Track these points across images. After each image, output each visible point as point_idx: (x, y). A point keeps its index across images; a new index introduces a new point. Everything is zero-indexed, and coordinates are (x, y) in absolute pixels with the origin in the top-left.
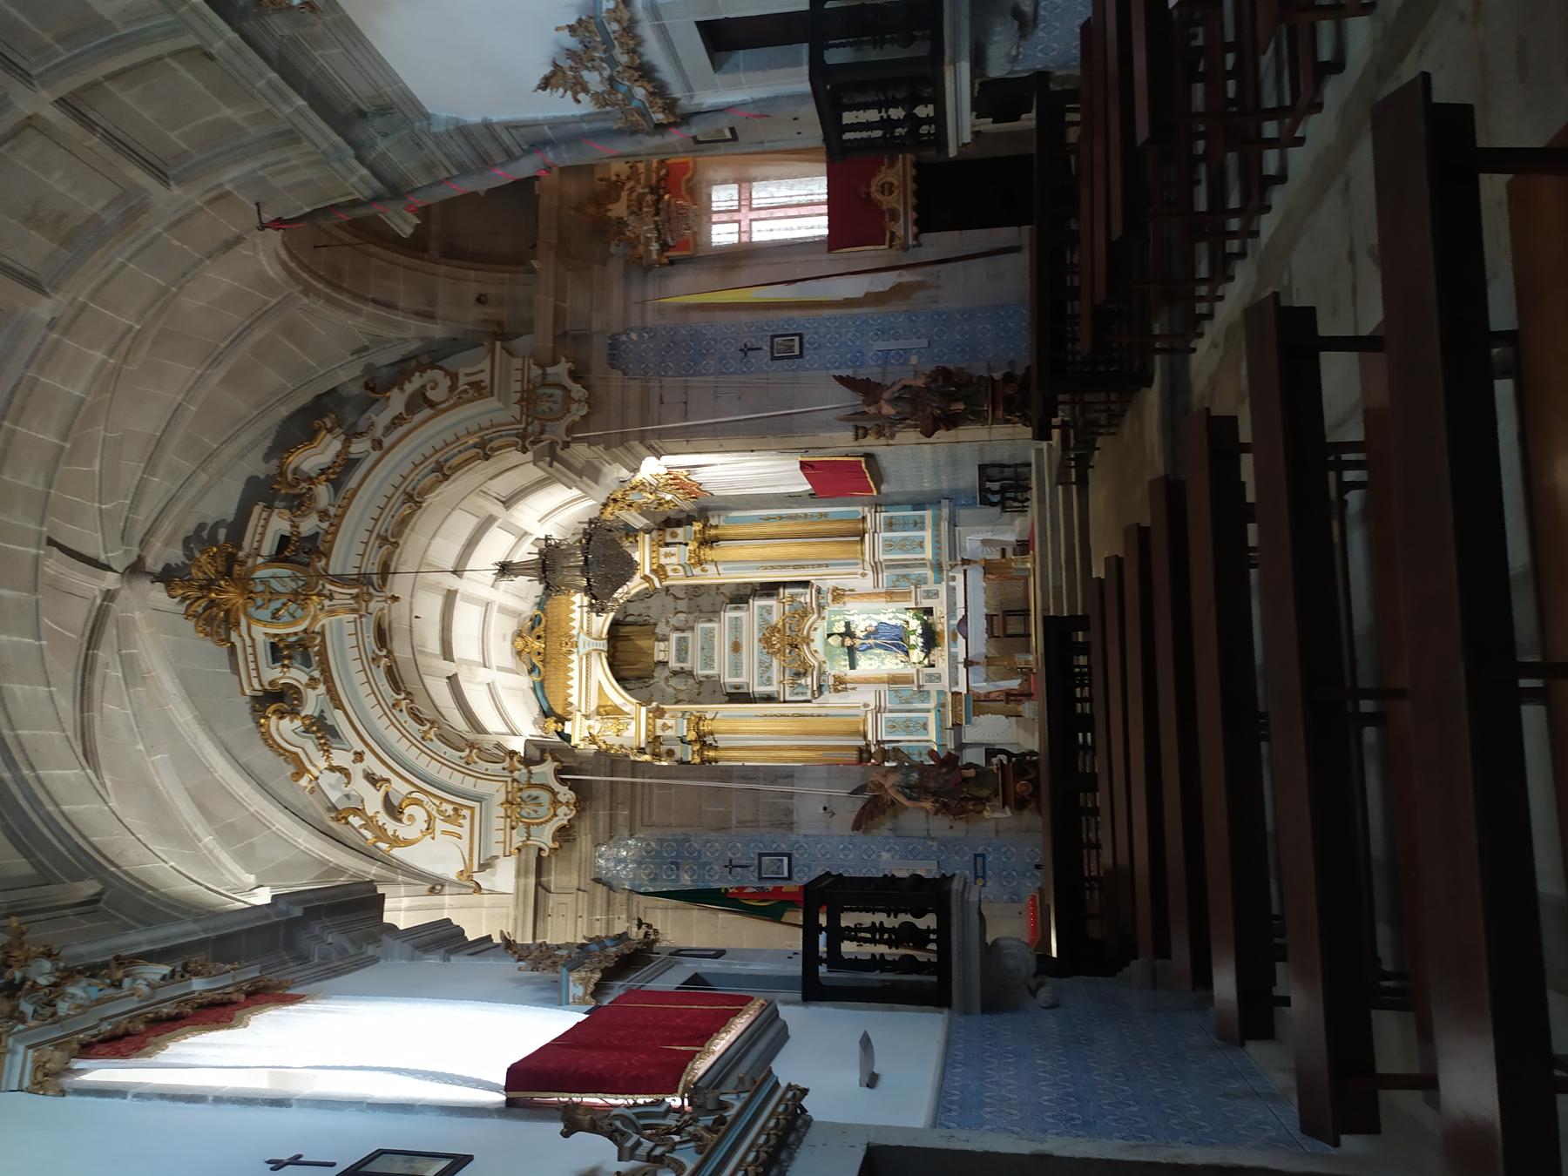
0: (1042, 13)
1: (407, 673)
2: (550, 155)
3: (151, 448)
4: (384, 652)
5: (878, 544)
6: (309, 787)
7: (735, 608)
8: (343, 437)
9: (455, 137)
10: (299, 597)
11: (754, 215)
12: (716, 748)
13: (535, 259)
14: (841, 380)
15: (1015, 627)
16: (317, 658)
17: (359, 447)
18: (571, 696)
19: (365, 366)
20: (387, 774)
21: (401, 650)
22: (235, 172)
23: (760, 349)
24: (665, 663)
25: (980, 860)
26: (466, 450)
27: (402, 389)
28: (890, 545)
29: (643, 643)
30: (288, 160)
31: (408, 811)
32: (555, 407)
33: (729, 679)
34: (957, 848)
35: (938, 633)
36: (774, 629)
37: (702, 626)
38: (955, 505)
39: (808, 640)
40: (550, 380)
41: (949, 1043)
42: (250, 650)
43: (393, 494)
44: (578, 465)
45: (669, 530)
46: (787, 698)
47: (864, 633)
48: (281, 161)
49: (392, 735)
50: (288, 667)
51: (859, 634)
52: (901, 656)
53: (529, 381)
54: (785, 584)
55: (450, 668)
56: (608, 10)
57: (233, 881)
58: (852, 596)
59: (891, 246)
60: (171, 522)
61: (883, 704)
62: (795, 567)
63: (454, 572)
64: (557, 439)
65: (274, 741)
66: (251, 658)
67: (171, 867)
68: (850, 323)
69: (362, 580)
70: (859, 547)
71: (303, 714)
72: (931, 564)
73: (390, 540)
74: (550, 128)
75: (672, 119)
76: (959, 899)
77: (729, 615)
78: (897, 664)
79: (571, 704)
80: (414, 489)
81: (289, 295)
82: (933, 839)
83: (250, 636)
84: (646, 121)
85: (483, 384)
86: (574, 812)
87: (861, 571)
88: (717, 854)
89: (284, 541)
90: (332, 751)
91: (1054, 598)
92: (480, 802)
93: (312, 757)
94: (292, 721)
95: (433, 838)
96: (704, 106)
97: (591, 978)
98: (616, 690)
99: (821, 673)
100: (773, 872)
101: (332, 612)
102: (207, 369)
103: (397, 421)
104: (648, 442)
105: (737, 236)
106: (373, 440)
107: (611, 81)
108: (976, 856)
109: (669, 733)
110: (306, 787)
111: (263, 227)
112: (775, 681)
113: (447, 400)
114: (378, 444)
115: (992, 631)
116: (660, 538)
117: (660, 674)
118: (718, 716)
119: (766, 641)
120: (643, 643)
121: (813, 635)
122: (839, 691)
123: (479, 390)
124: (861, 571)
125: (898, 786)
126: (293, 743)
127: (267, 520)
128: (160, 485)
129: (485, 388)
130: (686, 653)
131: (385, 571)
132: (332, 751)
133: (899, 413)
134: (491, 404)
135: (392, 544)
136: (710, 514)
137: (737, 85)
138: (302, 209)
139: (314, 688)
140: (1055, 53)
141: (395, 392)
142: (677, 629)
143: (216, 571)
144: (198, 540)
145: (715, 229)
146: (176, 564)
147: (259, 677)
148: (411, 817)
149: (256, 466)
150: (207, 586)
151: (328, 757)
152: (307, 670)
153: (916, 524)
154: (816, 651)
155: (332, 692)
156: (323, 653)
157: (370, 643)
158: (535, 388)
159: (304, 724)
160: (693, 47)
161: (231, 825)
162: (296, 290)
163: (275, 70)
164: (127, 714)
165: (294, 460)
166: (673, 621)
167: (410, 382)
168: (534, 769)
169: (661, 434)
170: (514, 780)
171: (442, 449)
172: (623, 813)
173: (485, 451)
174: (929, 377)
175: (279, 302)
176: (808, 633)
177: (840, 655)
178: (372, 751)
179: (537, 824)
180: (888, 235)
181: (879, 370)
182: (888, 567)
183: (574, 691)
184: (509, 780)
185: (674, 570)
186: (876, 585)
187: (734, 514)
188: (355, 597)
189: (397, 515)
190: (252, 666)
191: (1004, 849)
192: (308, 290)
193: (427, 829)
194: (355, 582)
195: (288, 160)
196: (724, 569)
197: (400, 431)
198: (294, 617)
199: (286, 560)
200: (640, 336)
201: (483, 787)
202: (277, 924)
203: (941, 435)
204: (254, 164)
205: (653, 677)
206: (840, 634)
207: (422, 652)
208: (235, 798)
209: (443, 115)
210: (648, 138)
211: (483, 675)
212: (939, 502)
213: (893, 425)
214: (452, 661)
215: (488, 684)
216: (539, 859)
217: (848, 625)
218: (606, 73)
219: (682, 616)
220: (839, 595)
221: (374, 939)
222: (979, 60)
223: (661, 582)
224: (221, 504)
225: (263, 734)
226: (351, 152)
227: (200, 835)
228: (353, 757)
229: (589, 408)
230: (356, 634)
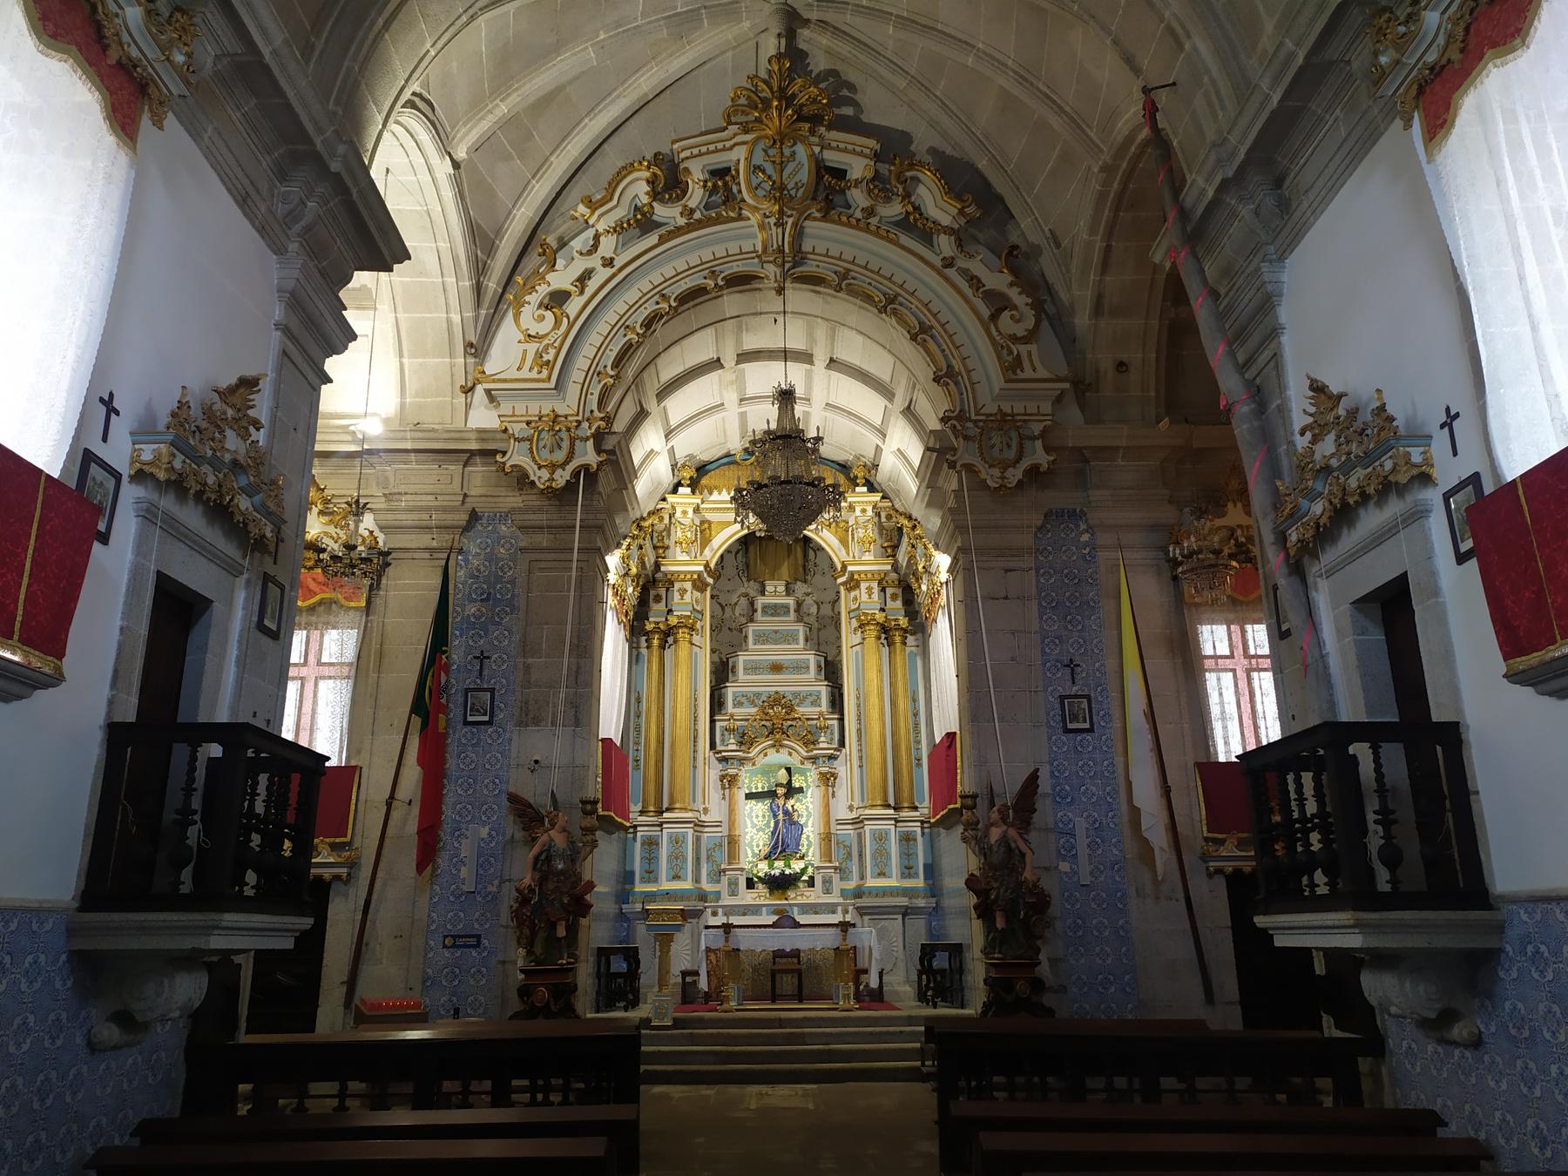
0: (1457, 1052)
1: (706, 311)
2: (1244, 409)
3: (924, 21)
4: (721, 283)
5: (882, 823)
6: (577, 215)
7: (819, 666)
8: (956, 226)
9: (1259, 294)
10: (779, 193)
11: (1241, 674)
12: (662, 647)
13: (1171, 422)
14: (1033, 778)
15: (787, 983)
16: (714, 215)
17: (945, 244)
18: (720, 494)
19: (1039, 246)
20: (589, 291)
21: (731, 302)
22: (1203, 48)
23: (1073, 682)
24: (763, 592)
25: (473, 941)
26: (946, 357)
27: (1011, 285)
28: (881, 837)
29: (785, 570)
30: (1223, 108)
31: (549, 314)
32: (996, 452)
33: (742, 660)
34: (489, 915)
36: (790, 708)
37: (801, 630)
38: (930, 914)
39: (778, 746)
40: (1027, 444)
41: (39, 912)
42: (720, 146)
43: (894, 283)
44: (940, 482)
45: (899, 591)
46: (718, 724)
48: (1220, 100)
49: (632, 295)
50: (705, 186)
51: (792, 802)
52: (767, 849)
53: (1025, 421)
54: (841, 720)
55: (729, 359)
56: (1409, 454)
57: (459, 135)
58: (826, 796)
59: (1206, 839)
60: (850, 52)
61: (707, 829)
62: (859, 730)
63: (832, 360)
64: (958, 454)
65: (625, 177)
66: (712, 147)
67: (428, 51)
68: (1108, 789)
69: (799, 257)
70: (879, 802)
71: (654, 204)
73: (844, 282)
74: (1278, 406)
75: (1292, 553)
76: (210, 923)
77: (812, 659)
78: (758, 846)
79: (711, 493)
80: (901, 304)
81: (1101, 151)
82: (500, 886)
83: (735, 145)
84: (1286, 519)
85: (1018, 371)
86: (542, 487)
88: (496, 643)
89: (840, 174)
90: (615, 236)
91: (790, 1033)
92: (555, 389)
93: (606, 216)
94: (647, 193)
95: (519, 342)
96: (1314, 594)
97: (160, 468)
98: (724, 543)
99: (742, 761)
100: (473, 704)
101: (762, 227)
102: (1013, 71)
103: (975, 282)
104: (961, 556)
105: (1212, 653)
106: (953, 258)
107: (1326, 470)
108: (478, 937)
109: (677, 596)
110: (576, 211)
111: (1146, 91)
112: (735, 710)
113: (1000, 334)
114: (949, 263)
115: (781, 957)
116: (890, 582)
117: (751, 588)
118: (696, 649)
119: (777, 700)
120: (785, 570)
121: (784, 751)
122: (722, 781)
123: (1013, 367)
125: (550, 847)
126: (622, 199)
127: (861, 154)
128: (887, 35)
129: (1015, 373)
130: (772, 615)
131: (814, 280)
132: (615, 236)
133: (991, 848)
134: (998, 381)
135: (840, 284)
136: (919, 635)
137: (1340, 633)
138: (1176, 137)
139: (681, 214)
140: (1409, 1067)
141: (1007, 277)
142: (799, 604)
143: (802, 106)
144: (838, 87)
145: (1221, 630)
146: (809, 64)
147: (693, 156)
148: (542, 318)
149: (923, 140)
150: (787, 99)
151: (608, 232)
152: (701, 207)
153: (909, 868)
154: (766, 755)
155: (679, 231)
156: (719, 220)
157: (732, 267)
158: (1017, 428)
159: (645, 205)
160: (1375, 573)
161: (529, 137)
162: (1106, 157)
163: (1307, 58)
164: (636, 19)
165: (927, 176)
166: (809, 600)
167: (1020, 294)
168: (590, 443)
169: (968, 570)
170: (579, 423)
171: (946, 331)
172: (544, 540)
173: (945, 377)
174: (1035, 885)
175: (1091, 140)
176: (786, 746)
177: (768, 781)
178: (614, 276)
179: (531, 448)
180: (1220, 836)
181: (1051, 825)
182: (859, 835)
184: (580, 418)
185: (855, 599)
186: (840, 822)
188: (781, 250)
189: (871, 288)
190: (704, 149)
191: (484, 970)
192: (1108, 169)
193: (529, 335)
194: (797, 248)
195: (1223, 108)
196: (857, 652)
197: (964, 285)
198: (756, 188)
199: (819, 177)
200: (1086, 544)
201: (573, 391)
202: (307, 139)
203: (973, 900)
204: (1214, 69)
205: (749, 581)
206: (790, 782)
207: (740, 329)
208: (563, 140)
209: (1285, 278)
210: (1271, 525)
211: (731, 397)
212: (933, 896)
213: (978, 841)
214: (738, 363)
215: (722, 404)
216: (493, 453)
217: (801, 790)
218: (1334, 463)
219: (814, 610)
220: (828, 779)
221: (315, 249)
222: (1382, 960)
223: (841, 584)
224: (879, 107)
225: (632, 164)
226: (1230, 174)
227: (508, 101)
228: (608, 256)
229: (995, 488)
230: (741, 253)
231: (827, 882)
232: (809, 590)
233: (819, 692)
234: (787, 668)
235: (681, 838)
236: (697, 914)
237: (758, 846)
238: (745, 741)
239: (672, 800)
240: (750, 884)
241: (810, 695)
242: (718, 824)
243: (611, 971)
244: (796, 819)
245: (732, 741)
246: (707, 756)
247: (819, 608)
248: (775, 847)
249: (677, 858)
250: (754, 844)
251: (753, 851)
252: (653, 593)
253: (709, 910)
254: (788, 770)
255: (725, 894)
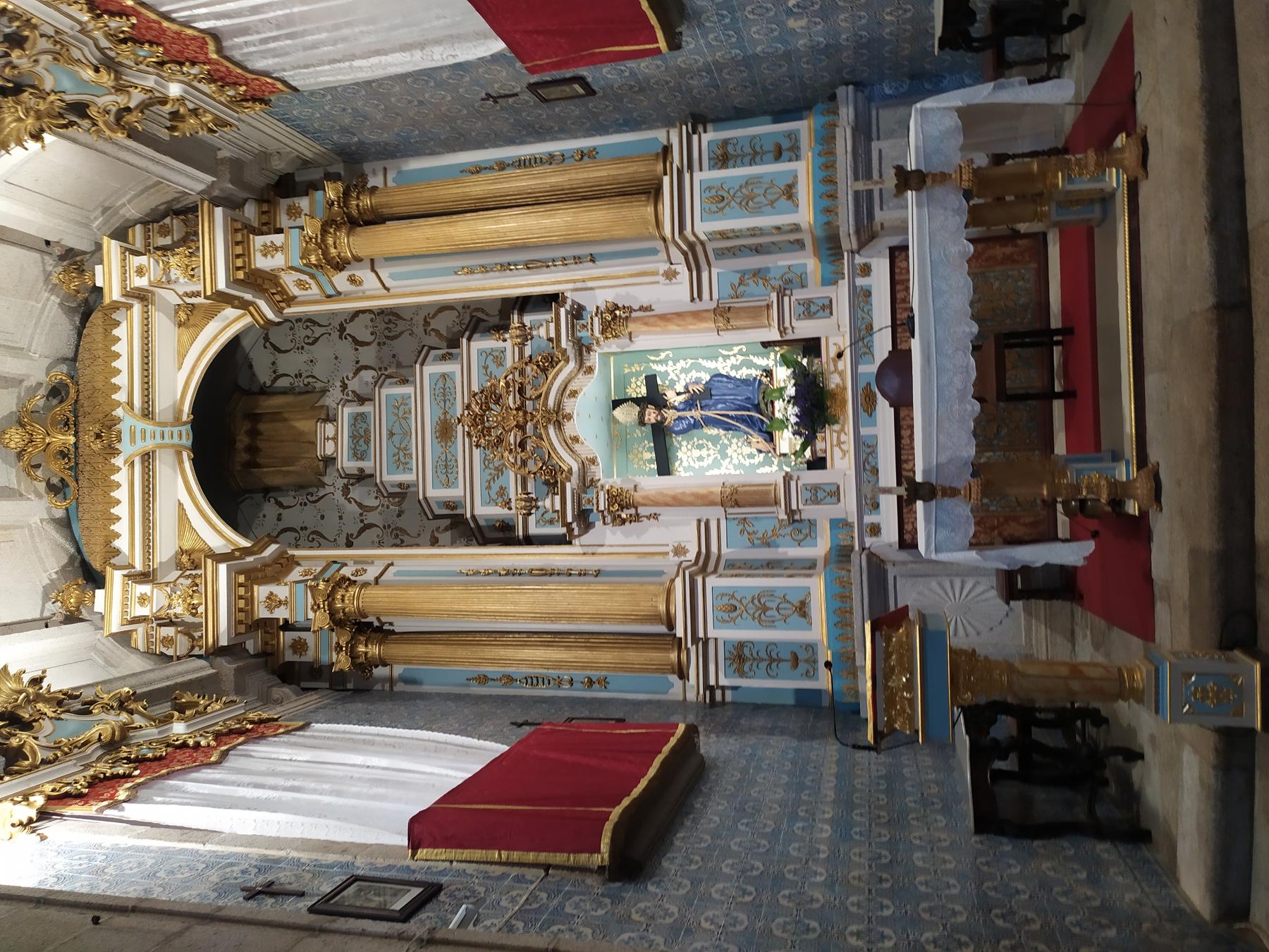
18: (118, 536)
28: (719, 200)
29: (303, 425)
33: (435, 493)
35: (833, 395)
39: (558, 417)
45: (284, 203)
46: (533, 530)
47: (682, 398)
51: (672, 397)
52: (757, 439)
61: (714, 549)
70: (650, 209)
72: (816, 241)
78: (751, 456)
87: (664, 267)
99: (587, 483)
118: (389, 576)
120: (303, 425)
121: (569, 405)
122: (623, 522)
124: (664, 267)
130: (367, 442)
154: (576, 439)
182: (722, 254)
183: (121, 527)
186: (697, 293)
187: (415, 164)
205: (323, 485)
206: (637, 401)
212: (833, 97)
217: (651, 381)
231: (809, 310)
232: (338, 384)
233: (481, 352)
234: (445, 413)
235: (725, 600)
236: (877, 568)
237: (751, 456)
238: (553, 480)
239: (654, 618)
240: (818, 463)
241: (486, 368)
242: (704, 528)
243: (1016, 769)
244: (700, 387)
245: (548, 503)
246: (579, 550)
247: (366, 368)
248: (750, 422)
249: (765, 609)
250: (747, 462)
251: (761, 465)
252: (289, 656)
253: (869, 541)
254: (616, 404)
255: (834, 511)
